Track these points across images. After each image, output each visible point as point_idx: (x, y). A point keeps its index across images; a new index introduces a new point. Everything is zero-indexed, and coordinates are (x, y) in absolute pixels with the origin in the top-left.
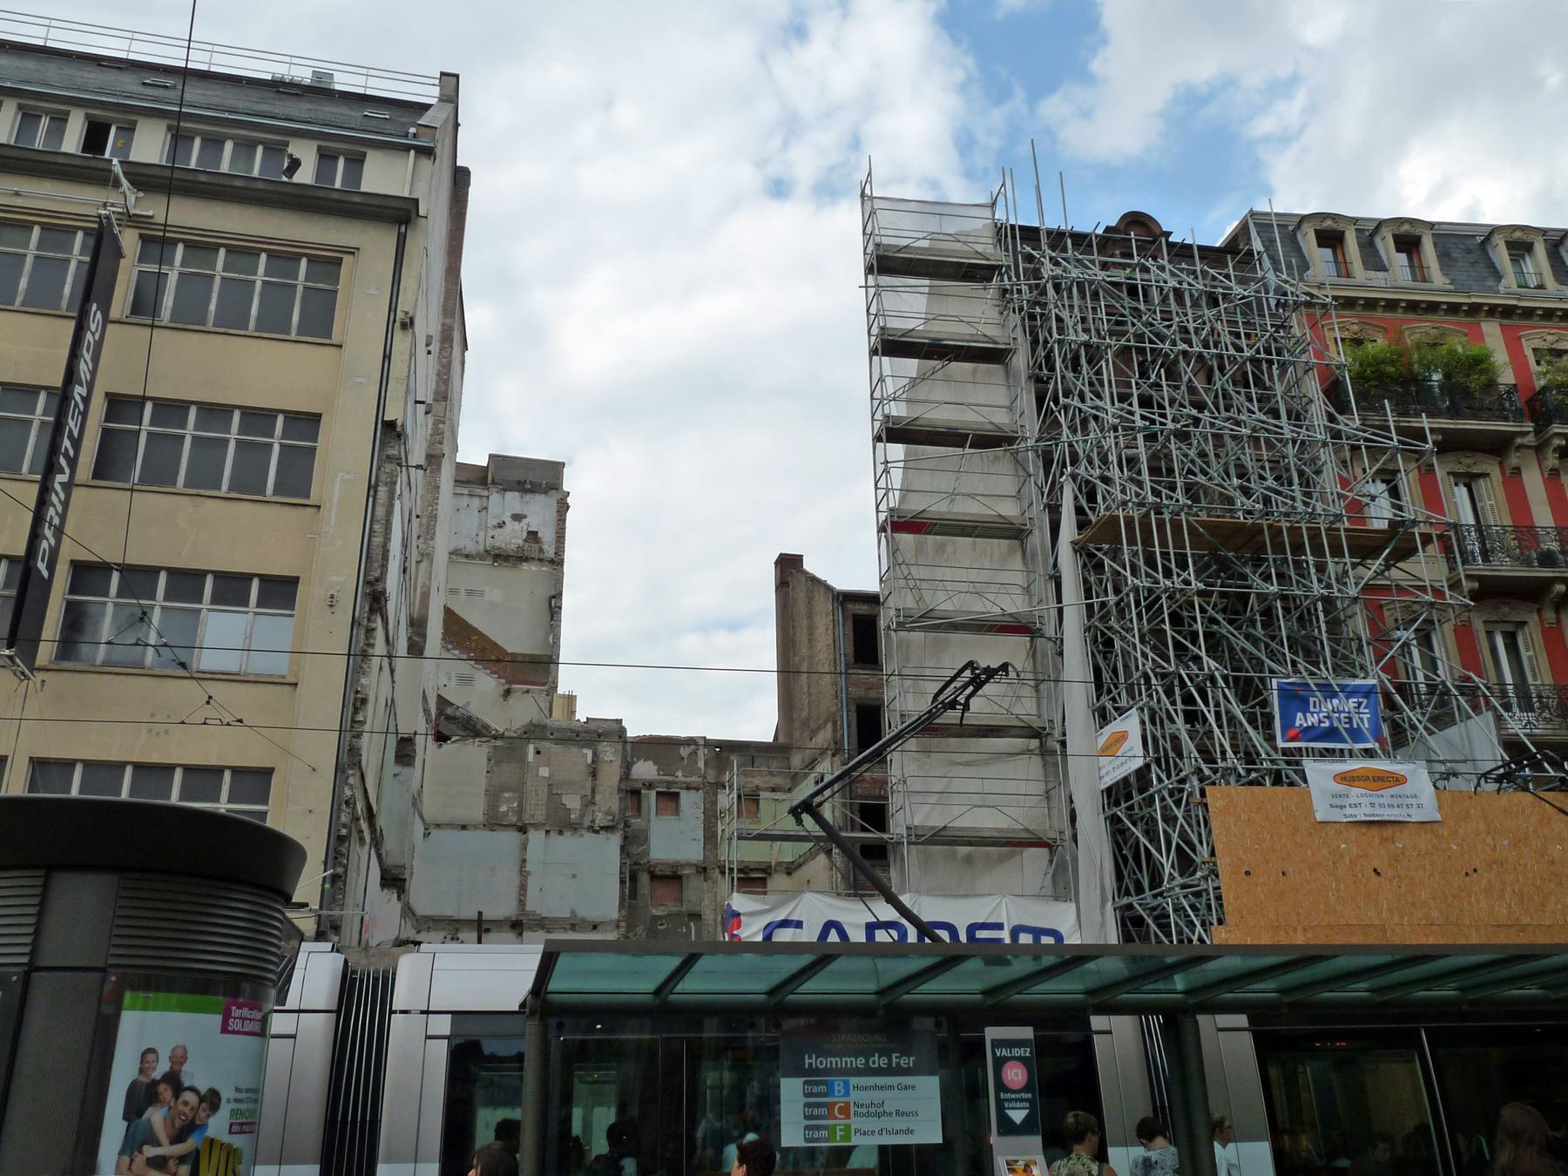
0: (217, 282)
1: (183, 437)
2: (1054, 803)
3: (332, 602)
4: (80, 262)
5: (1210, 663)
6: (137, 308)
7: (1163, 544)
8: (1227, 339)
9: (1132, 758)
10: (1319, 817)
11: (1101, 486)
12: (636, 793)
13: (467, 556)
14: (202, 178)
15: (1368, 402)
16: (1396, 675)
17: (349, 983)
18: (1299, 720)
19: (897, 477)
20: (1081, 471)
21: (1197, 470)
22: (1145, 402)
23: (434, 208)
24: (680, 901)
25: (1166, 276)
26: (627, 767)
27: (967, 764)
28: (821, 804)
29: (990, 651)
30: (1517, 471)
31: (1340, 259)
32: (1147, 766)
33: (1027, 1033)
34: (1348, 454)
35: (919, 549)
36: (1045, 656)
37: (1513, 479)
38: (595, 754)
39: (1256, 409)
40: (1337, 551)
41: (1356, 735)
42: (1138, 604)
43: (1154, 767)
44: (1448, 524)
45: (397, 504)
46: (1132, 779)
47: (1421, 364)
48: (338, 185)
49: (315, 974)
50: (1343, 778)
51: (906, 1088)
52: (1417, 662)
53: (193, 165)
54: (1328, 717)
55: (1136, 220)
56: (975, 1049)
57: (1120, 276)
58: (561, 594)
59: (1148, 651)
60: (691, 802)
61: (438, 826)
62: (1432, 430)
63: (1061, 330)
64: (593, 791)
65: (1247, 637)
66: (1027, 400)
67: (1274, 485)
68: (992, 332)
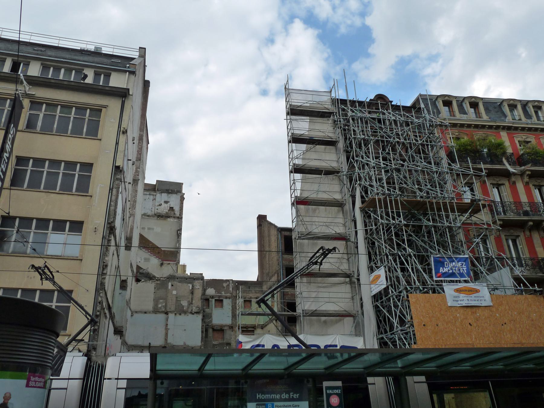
0: (57, 117)
1: (43, 172)
2: (355, 301)
3: (96, 230)
4: (8, 110)
5: (409, 250)
6: (28, 126)
7: (392, 208)
8: (412, 137)
9: (382, 284)
10: (449, 304)
11: (369, 188)
12: (207, 300)
13: (148, 216)
14: (53, 81)
15: (462, 159)
16: (475, 254)
17: (88, 369)
18: (441, 270)
19: (298, 185)
20: (363, 183)
21: (403, 183)
22: (385, 159)
23: (136, 92)
24: (223, 338)
25: (391, 116)
26: (204, 290)
27: (324, 287)
28: (268, 300)
29: (329, 245)
30: (514, 183)
31: (451, 110)
32: (388, 287)
33: (339, 384)
34: (456, 177)
35: (307, 211)
36: (351, 248)
37: (513, 186)
38: (193, 286)
39: (423, 161)
40: (453, 211)
41: (462, 275)
42: (383, 229)
43: (390, 287)
44: (491, 201)
45: (120, 196)
46: (383, 292)
47: (480, 146)
48: (101, 84)
49: (74, 365)
50: (457, 290)
51: (296, 406)
52: (482, 249)
53: (50, 77)
54: (451, 269)
55: (380, 97)
56: (319, 391)
57: (374, 116)
58: (181, 229)
59: (387, 246)
60: (227, 303)
61: (136, 312)
62: (485, 169)
63: (355, 134)
64: (192, 300)
65: (422, 241)
66: (343, 158)
67: (430, 188)
68: (330, 135)
